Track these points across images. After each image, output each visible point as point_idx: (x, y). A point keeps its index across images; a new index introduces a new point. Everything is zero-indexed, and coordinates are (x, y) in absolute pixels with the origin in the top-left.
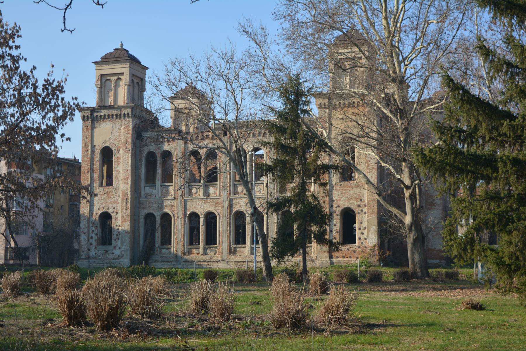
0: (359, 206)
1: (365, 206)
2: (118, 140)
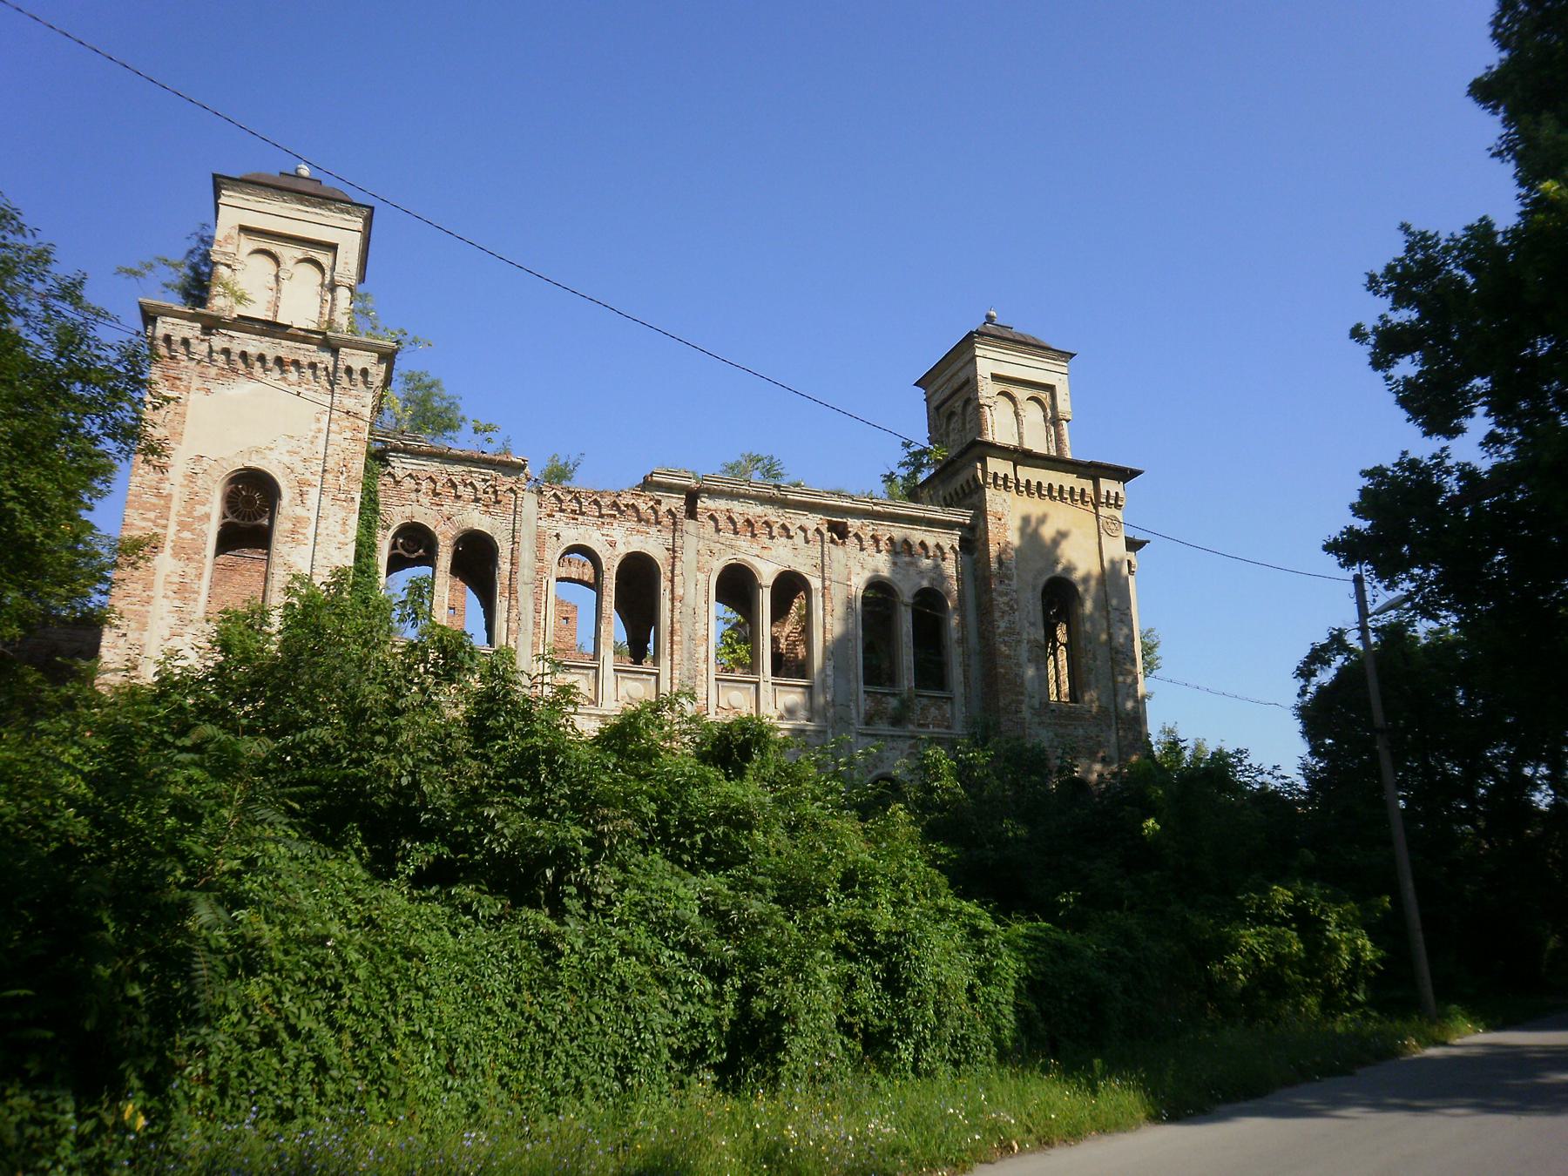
2: (305, 454)
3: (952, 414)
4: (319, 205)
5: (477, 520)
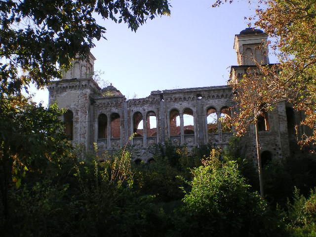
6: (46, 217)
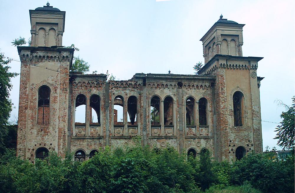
0: (248, 145)
1: (252, 145)
3: (210, 47)
4: (53, 14)
5: (95, 91)
6: (36, 161)
